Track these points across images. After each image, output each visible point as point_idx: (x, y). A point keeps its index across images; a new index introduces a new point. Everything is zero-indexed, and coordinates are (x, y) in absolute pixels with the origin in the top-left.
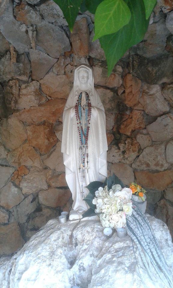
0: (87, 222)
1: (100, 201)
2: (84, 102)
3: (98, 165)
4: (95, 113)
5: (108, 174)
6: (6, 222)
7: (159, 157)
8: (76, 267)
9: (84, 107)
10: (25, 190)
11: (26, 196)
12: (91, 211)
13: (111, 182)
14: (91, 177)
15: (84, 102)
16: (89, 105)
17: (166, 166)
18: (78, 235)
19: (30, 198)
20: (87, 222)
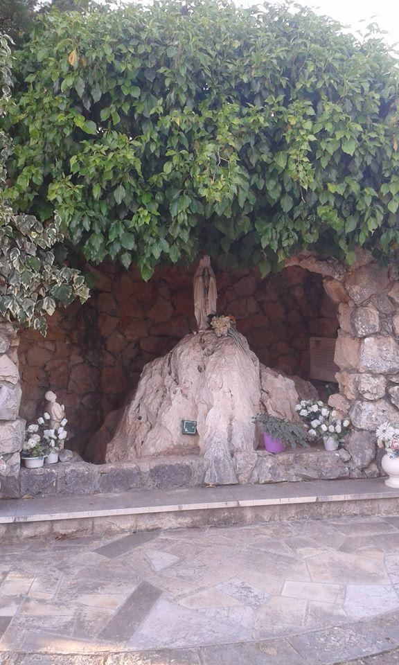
0: (208, 333)
1: (215, 322)
2: (206, 274)
3: (212, 307)
4: (212, 279)
5: (217, 309)
6: (112, 364)
7: (242, 308)
8: (206, 350)
9: (205, 276)
10: (129, 338)
11: (129, 343)
12: (210, 328)
13: (220, 313)
14: (209, 312)
15: (206, 274)
16: (209, 275)
17: (247, 315)
18: (205, 338)
19: (133, 344)
20: (208, 333)
